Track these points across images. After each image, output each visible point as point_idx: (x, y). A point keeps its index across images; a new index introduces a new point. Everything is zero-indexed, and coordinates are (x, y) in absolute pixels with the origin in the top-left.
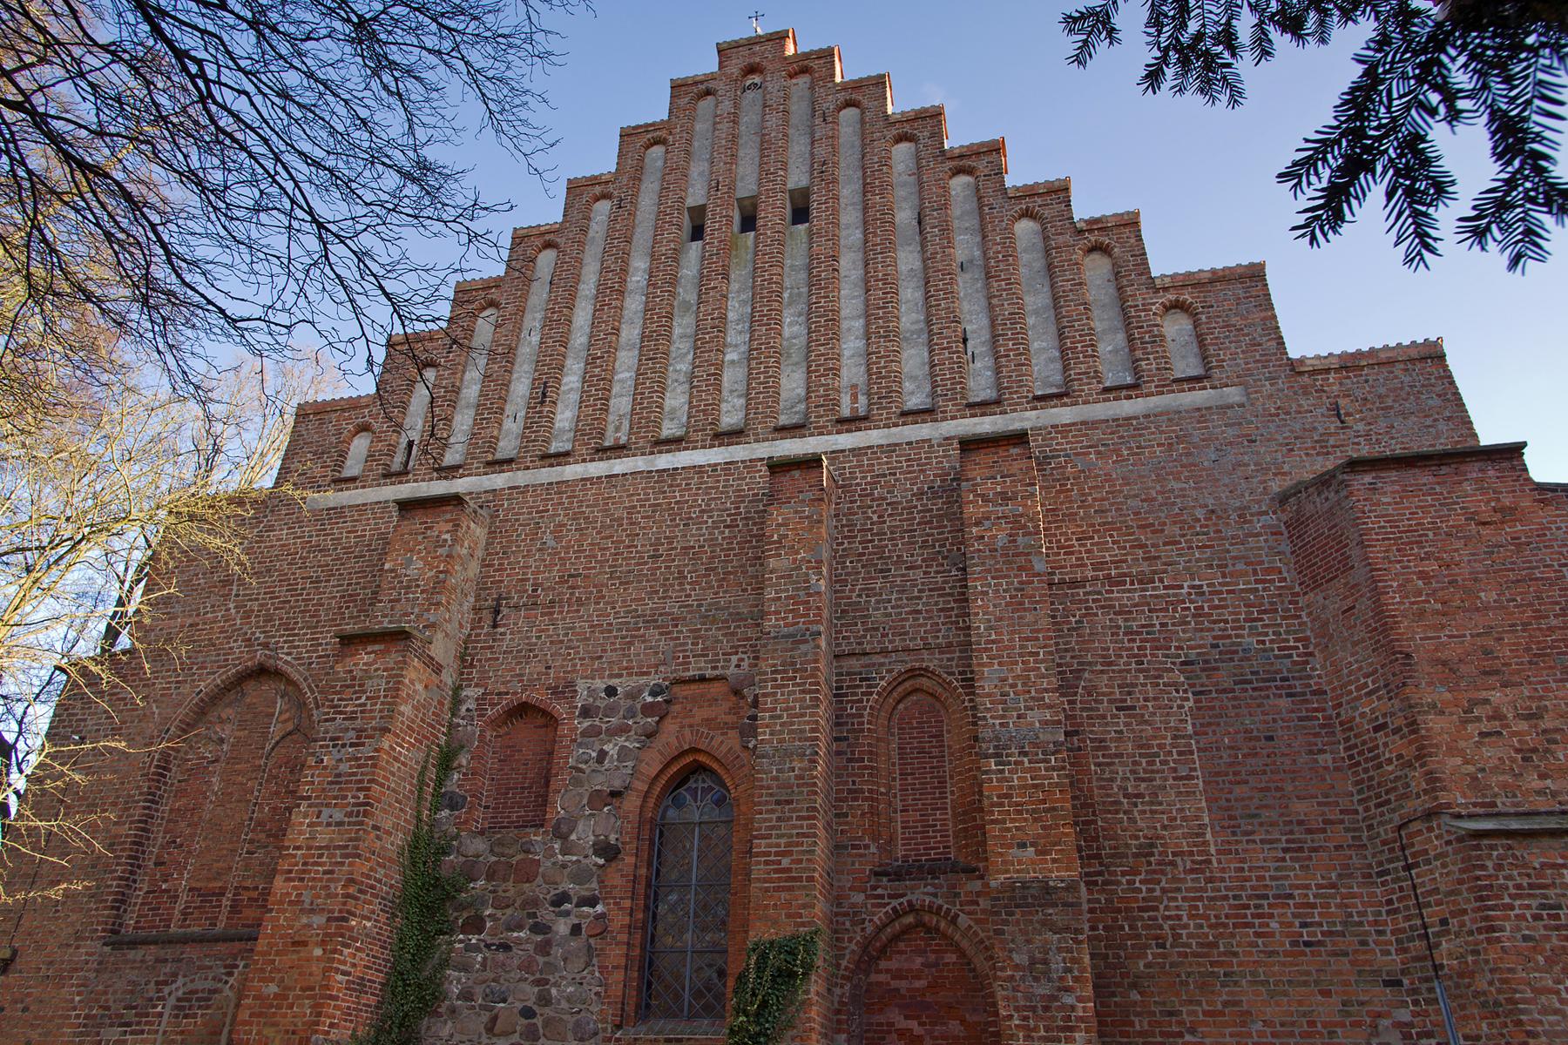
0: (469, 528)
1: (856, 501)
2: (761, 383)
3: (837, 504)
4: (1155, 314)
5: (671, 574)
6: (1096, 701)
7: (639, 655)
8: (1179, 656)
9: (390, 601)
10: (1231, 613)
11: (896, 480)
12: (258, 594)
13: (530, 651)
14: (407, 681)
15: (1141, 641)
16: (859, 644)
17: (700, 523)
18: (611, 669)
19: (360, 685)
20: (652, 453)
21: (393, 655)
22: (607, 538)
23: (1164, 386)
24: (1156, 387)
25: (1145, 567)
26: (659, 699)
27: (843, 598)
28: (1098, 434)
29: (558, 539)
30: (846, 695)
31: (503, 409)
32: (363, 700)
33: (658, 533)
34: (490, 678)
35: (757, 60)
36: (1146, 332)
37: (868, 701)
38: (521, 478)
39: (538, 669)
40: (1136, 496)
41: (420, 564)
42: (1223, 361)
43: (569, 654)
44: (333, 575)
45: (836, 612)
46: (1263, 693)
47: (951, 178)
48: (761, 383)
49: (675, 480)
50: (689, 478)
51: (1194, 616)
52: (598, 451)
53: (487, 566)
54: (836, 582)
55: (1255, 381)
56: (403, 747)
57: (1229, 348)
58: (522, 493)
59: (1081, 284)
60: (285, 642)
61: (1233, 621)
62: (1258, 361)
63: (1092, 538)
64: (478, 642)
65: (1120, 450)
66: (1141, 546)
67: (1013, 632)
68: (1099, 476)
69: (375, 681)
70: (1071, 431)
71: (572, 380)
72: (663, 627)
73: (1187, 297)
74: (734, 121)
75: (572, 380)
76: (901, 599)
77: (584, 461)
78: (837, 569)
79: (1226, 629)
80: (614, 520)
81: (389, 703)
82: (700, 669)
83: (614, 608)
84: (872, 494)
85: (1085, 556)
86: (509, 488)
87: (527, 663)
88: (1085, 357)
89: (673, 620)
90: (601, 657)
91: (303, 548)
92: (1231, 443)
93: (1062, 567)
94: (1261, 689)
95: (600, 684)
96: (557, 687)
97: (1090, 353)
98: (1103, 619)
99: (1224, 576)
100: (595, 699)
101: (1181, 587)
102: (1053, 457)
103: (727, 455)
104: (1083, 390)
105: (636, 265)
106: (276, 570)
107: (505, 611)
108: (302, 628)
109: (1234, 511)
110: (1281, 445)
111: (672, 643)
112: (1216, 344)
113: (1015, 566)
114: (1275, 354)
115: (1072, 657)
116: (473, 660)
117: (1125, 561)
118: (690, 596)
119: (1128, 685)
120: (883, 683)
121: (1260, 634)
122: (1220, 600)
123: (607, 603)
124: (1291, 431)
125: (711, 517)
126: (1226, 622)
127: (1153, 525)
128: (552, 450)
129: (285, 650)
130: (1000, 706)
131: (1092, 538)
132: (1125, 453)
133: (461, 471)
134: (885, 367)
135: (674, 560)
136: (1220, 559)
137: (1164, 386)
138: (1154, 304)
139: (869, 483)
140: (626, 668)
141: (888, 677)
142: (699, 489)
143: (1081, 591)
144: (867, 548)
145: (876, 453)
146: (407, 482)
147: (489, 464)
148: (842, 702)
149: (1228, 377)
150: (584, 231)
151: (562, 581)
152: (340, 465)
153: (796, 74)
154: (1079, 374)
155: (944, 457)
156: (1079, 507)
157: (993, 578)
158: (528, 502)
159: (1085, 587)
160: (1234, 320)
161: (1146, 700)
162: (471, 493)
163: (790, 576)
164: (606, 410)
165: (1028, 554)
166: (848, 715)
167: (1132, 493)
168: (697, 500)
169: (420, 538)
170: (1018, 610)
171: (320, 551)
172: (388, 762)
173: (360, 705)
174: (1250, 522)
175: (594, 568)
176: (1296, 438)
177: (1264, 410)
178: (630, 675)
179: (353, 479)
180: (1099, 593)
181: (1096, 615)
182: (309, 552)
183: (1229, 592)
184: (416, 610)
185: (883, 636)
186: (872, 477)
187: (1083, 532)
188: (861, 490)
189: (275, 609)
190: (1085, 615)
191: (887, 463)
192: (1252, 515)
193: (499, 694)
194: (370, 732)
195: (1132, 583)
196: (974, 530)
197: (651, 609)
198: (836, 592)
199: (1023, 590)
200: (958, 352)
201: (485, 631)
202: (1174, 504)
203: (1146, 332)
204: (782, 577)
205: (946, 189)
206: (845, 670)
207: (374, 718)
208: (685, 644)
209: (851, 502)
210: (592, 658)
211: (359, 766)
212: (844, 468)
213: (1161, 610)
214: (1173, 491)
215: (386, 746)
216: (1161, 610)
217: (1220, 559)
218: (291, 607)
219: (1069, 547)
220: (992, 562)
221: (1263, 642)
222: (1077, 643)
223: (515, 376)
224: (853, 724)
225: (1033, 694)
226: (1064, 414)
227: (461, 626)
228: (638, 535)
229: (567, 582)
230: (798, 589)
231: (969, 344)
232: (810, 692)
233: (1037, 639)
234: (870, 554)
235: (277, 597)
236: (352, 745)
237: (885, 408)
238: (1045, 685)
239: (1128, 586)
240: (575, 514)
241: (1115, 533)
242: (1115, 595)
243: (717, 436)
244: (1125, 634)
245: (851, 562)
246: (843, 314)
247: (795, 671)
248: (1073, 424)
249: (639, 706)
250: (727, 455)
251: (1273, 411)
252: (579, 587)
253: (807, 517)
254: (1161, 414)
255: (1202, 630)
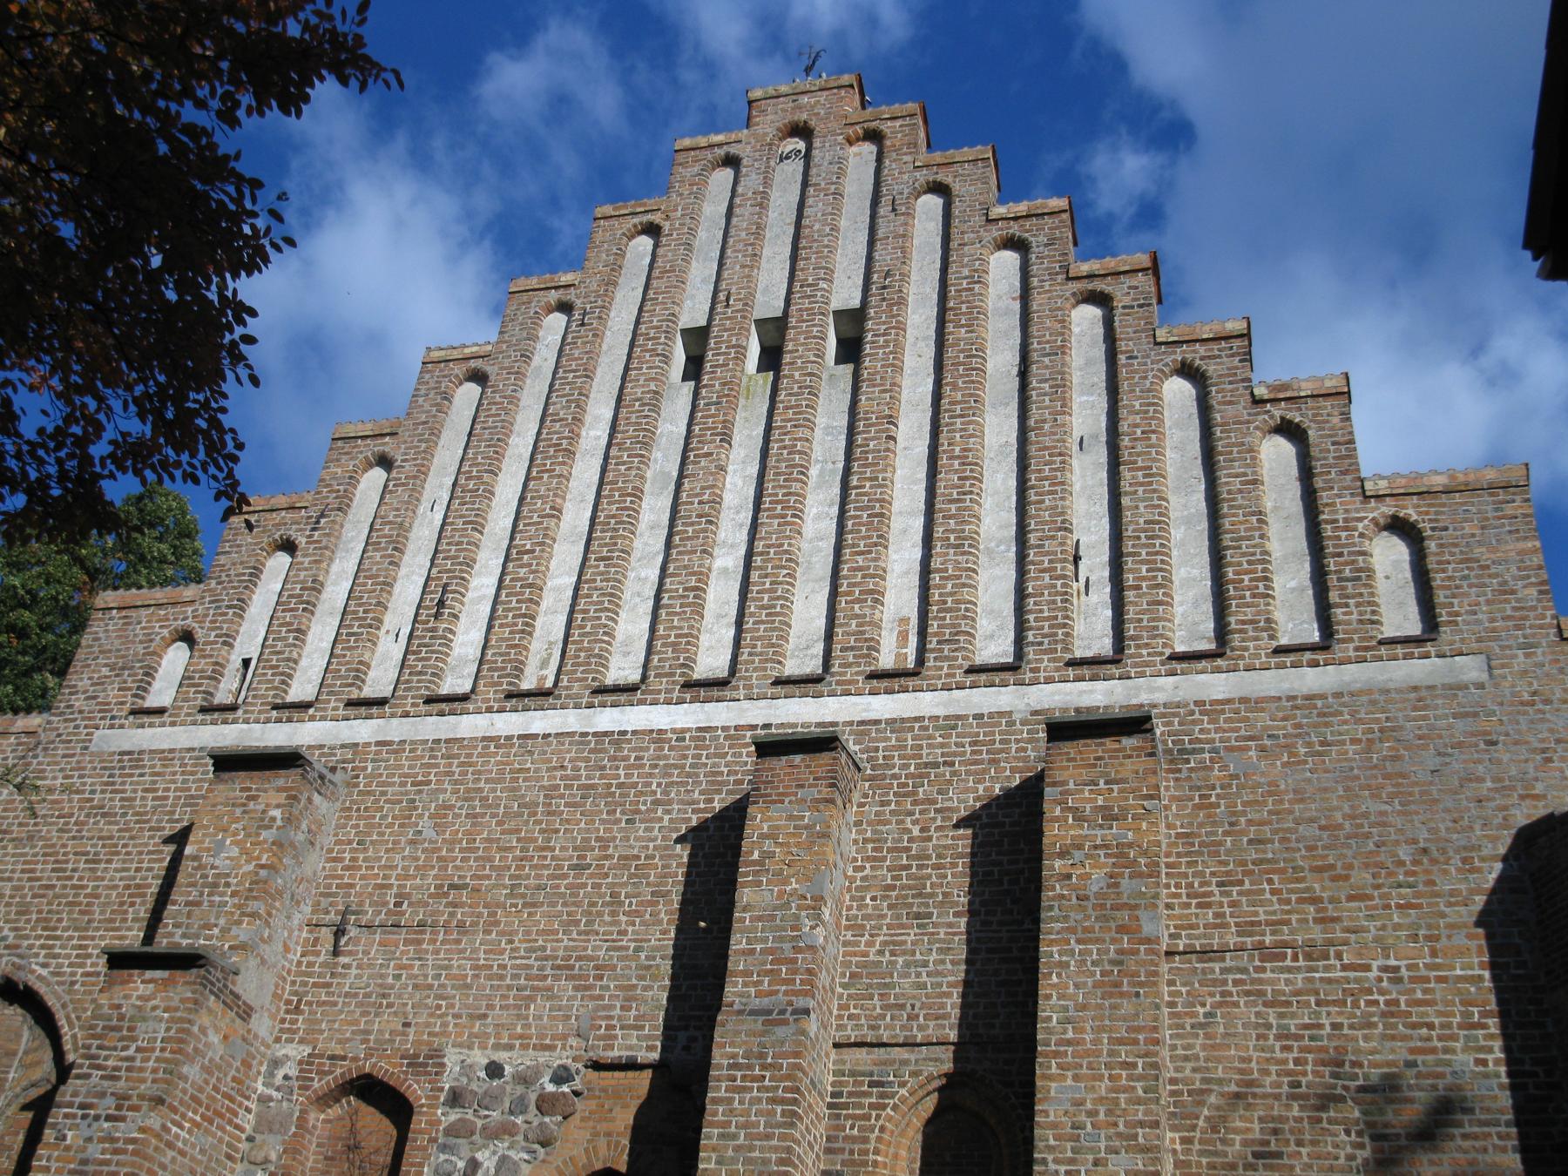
0: (310, 800)
1: (888, 803)
2: (763, 607)
3: (861, 805)
4: (1362, 535)
5: (602, 896)
6: (1224, 1141)
7: (540, 1018)
8: (1355, 1077)
9: (188, 904)
10: (1440, 1014)
11: (954, 773)
12: (13, 871)
13: (384, 996)
14: (195, 1029)
15: (1301, 1050)
16: (872, 1028)
17: (651, 821)
18: (498, 1036)
19: (130, 1029)
20: (590, 706)
21: (179, 988)
22: (511, 832)
23: (1367, 649)
24: (1357, 649)
25: (1317, 934)
26: (565, 1089)
27: (855, 954)
28: (1263, 720)
29: (439, 828)
30: (846, 1106)
31: (381, 621)
32: (131, 1052)
33: (588, 831)
34: (321, 1032)
35: (804, 116)
36: (1347, 563)
37: (878, 1117)
38: (394, 728)
39: (392, 1026)
40: (1312, 820)
41: (235, 851)
42: (1457, 614)
43: (439, 1007)
44: (118, 853)
45: (843, 975)
46: (1478, 1144)
47: (1074, 306)
48: (763, 607)
49: (620, 749)
50: (642, 749)
51: (1384, 1014)
52: (510, 696)
53: (334, 860)
54: (847, 928)
55: (1502, 648)
56: (181, 1127)
57: (1466, 595)
58: (396, 752)
59: (1255, 482)
60: (42, 947)
61: (1442, 1026)
62: (1509, 618)
63: (1241, 883)
64: (310, 975)
65: (1294, 745)
66: (1315, 900)
67: (1101, 1029)
68: (1259, 785)
69: (151, 1025)
70: (1223, 712)
71: (483, 583)
72: (580, 977)
73: (1411, 512)
74: (761, 205)
75: (483, 583)
76: (943, 962)
77: (489, 710)
78: (849, 908)
79: (1429, 1039)
80: (525, 805)
81: (166, 1061)
82: (630, 1048)
83: (511, 942)
84: (915, 793)
85: (1227, 910)
86: (378, 743)
87: (377, 1015)
88: (1254, 596)
89: (597, 968)
90: (485, 1016)
91: (81, 809)
92: (1460, 745)
93: (1191, 927)
94: (1476, 1137)
95: (480, 1058)
96: (416, 1056)
97: (1262, 590)
98: (1246, 1011)
99: (1434, 954)
100: (470, 1080)
101: (1367, 968)
102: (1194, 751)
103: (702, 716)
104: (1246, 649)
105: (597, 412)
106: (41, 838)
107: (353, 932)
108: (66, 929)
109: (1457, 851)
110: (1534, 751)
111: (591, 1005)
112: (1449, 588)
113: (1113, 925)
114: (1534, 608)
115: (1194, 1070)
116: (299, 1001)
117: (1287, 922)
118: (625, 933)
119: (1273, 1119)
120: (903, 1091)
121: (1481, 1049)
122: (1425, 991)
123: (499, 933)
124: (1551, 731)
125: (668, 812)
126: (1431, 1026)
127: (1332, 867)
128: (445, 690)
129: (41, 960)
130: (1069, 1145)
131: (1241, 883)
132: (1303, 750)
133: (311, 711)
134: (951, 594)
135: (607, 876)
136: (1429, 927)
137: (1367, 649)
138: (1360, 519)
139: (912, 776)
140: (521, 1037)
141: (912, 1082)
142: (656, 766)
143: (1217, 966)
144: (899, 878)
145: (926, 728)
146: (235, 721)
147: (351, 704)
148: (838, 1116)
149: (1462, 640)
150: (526, 357)
151: (439, 894)
152: (143, 688)
153: (858, 140)
154: (1243, 622)
155: (1029, 741)
156: (1226, 833)
157: (1079, 942)
158: (401, 767)
159: (1223, 960)
160: (1478, 551)
161: (1299, 1143)
162: (321, 747)
163: (772, 918)
164: (530, 634)
165: (1136, 907)
166: (846, 1138)
167: (1308, 815)
168: (649, 784)
169: (238, 811)
170: (1111, 995)
171: (104, 815)
172: (156, 1149)
173: (127, 1059)
174: (1479, 870)
175: (488, 877)
176: (1558, 741)
177: (1514, 694)
178: (524, 1047)
179: (160, 711)
180: (1244, 971)
181: (1236, 1004)
182: (88, 815)
183: (1440, 979)
184: (222, 922)
185: (909, 1018)
186: (917, 766)
187: (1228, 873)
188: (900, 785)
189: (34, 896)
190: (1220, 1005)
191: (942, 745)
192: (1482, 859)
193: (332, 1057)
194: (135, 1101)
195: (1295, 958)
196: (1058, 864)
197: (566, 948)
198: (845, 944)
199: (1120, 963)
200: (1064, 577)
201: (322, 958)
202: (1368, 836)
203: (1347, 563)
204: (760, 918)
205: (1064, 323)
206: (848, 1066)
207: (143, 1081)
208: (612, 1007)
209: (883, 804)
210: (471, 1016)
211: (116, 1152)
212: (877, 749)
213: (1334, 1003)
214: (1366, 815)
215: (157, 1126)
216: (1334, 1003)
217: (1429, 927)
218: (56, 896)
219: (1206, 895)
220: (1080, 917)
221: (1484, 1063)
222: (1204, 1046)
223: (403, 571)
224: (852, 1152)
225: (1121, 1127)
226: (1214, 684)
227: (287, 949)
228: (557, 831)
229: (446, 895)
230: (781, 939)
231: (1082, 565)
232: (783, 1101)
233: (1135, 1042)
234: (903, 888)
235: (39, 879)
236: (109, 1118)
237: (947, 658)
238: (1140, 1116)
239: (1288, 962)
240: (468, 791)
241: (1275, 878)
242: (1269, 975)
243: (689, 685)
244: (1278, 1037)
245: (873, 899)
246: (896, 507)
247: (764, 1067)
248: (1229, 701)
249: (533, 1097)
250: (702, 716)
251: (1526, 697)
252: (462, 905)
253: (806, 827)
254: (1360, 693)
255: (1393, 1038)
